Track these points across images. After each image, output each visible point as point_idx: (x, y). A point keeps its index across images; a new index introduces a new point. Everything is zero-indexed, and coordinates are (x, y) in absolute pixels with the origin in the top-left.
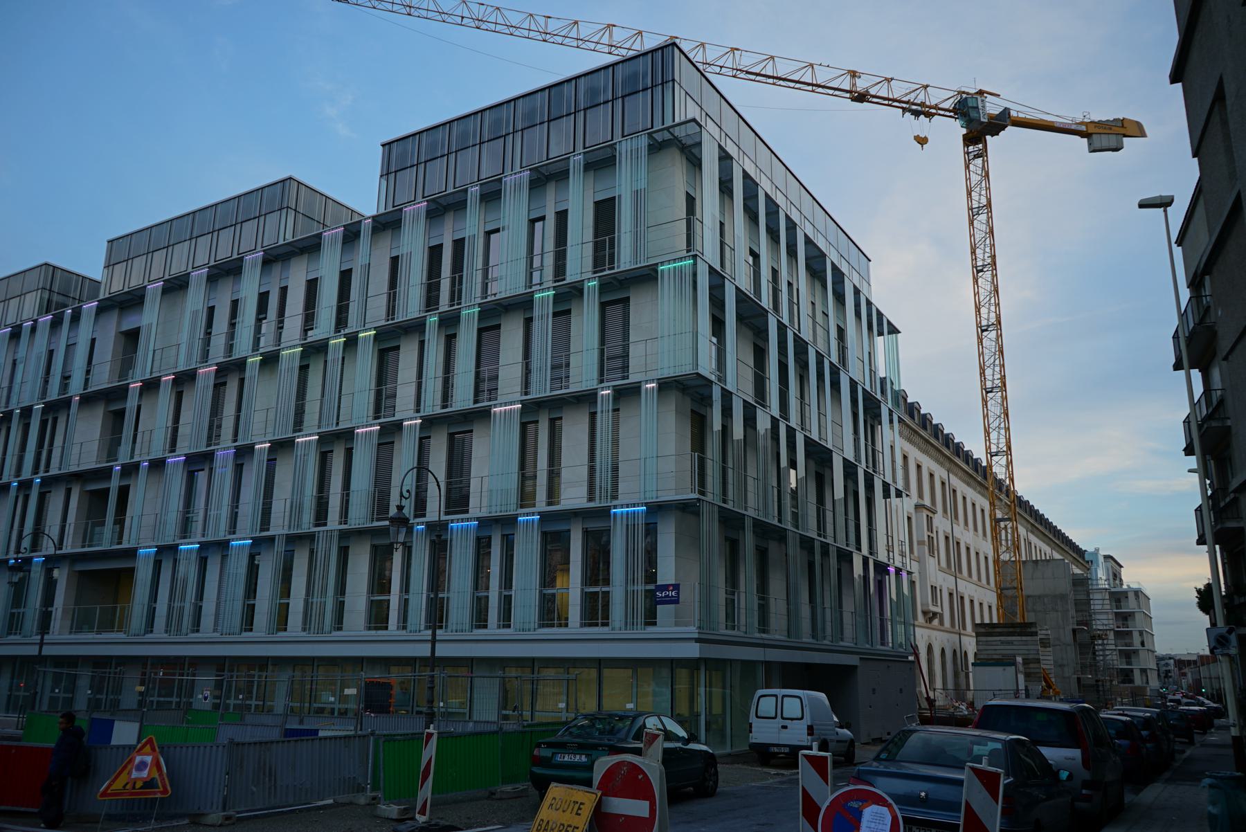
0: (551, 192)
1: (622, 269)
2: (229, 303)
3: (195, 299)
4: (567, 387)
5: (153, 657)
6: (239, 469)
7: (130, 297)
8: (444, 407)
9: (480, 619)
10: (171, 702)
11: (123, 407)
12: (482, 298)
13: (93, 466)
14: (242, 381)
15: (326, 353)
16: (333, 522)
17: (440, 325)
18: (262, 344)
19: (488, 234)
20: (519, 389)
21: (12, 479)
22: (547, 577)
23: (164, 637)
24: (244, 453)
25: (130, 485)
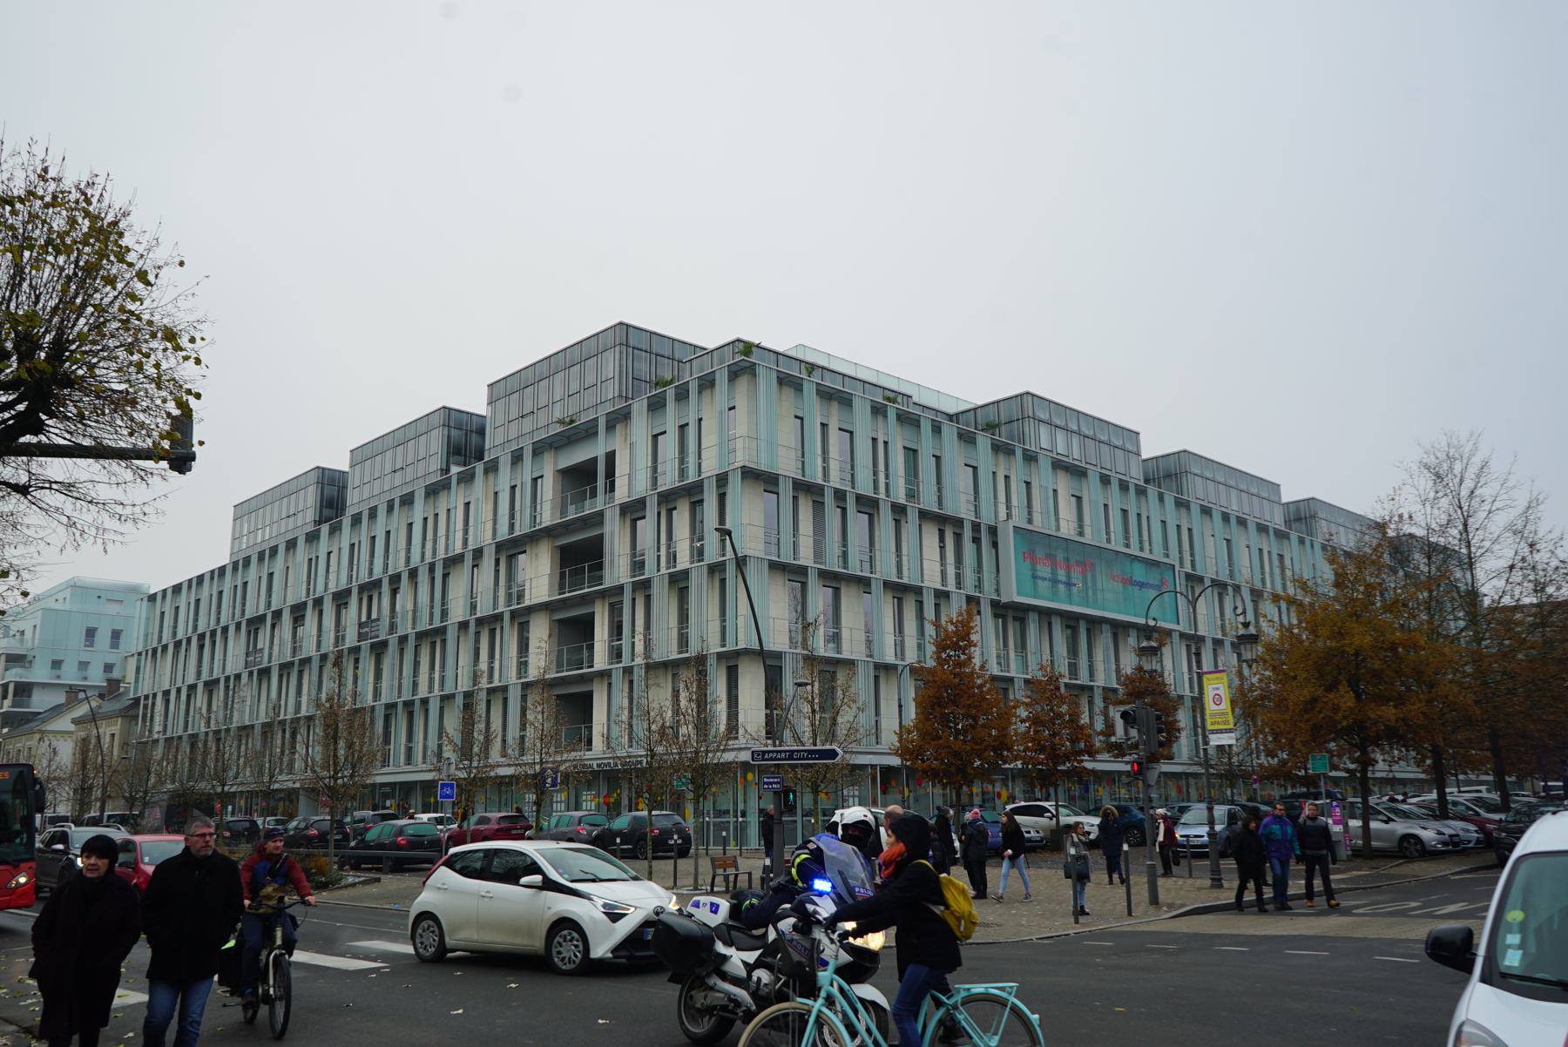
0: (443, 496)
1: (544, 525)
2: (445, 511)
3: (302, 551)
4: (675, 567)
5: (421, 781)
6: (402, 651)
7: (559, 438)
8: (431, 624)
9: (409, 760)
10: (1138, 793)
11: (599, 532)
12: (679, 482)
13: (546, 599)
14: (380, 593)
15: (381, 587)
16: (437, 692)
17: (333, 599)
18: (247, 612)
19: (655, 437)
20: (688, 558)
21: (221, 675)
22: (634, 709)
23: (422, 767)
24: (403, 640)
25: (594, 613)
